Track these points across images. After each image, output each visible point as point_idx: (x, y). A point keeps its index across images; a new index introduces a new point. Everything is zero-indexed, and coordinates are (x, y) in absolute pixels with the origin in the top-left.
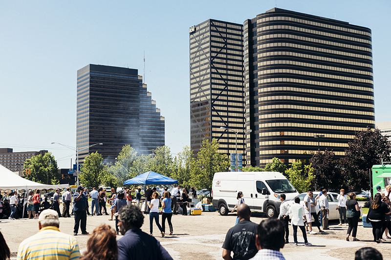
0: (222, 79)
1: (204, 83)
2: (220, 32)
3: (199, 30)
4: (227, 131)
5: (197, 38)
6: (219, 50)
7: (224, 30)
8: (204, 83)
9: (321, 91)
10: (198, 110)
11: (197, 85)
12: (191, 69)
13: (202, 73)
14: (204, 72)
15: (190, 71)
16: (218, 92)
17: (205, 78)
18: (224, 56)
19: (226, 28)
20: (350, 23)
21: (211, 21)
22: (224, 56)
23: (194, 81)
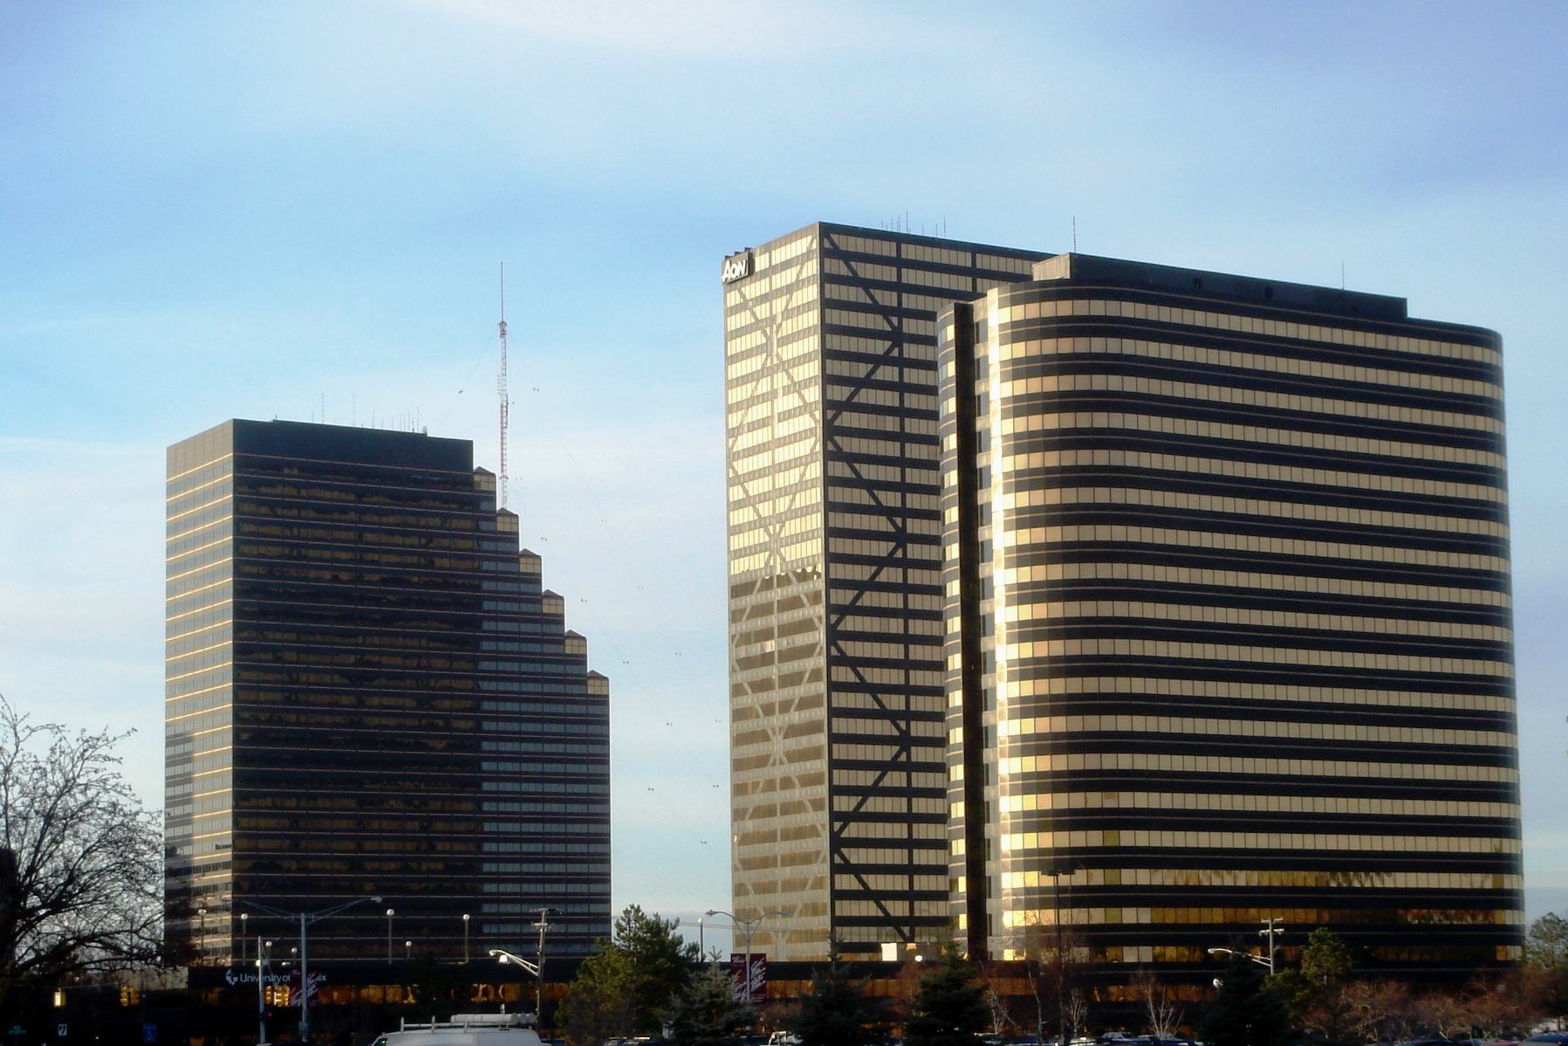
0: (878, 510)
1: (794, 527)
2: (867, 285)
3: (772, 270)
4: (895, 353)
5: (757, 310)
6: (862, 370)
7: (889, 274)
8: (794, 527)
9: (1319, 800)
10: (768, 862)
11: (759, 536)
12: (732, 456)
13: (783, 480)
14: (793, 476)
15: (730, 465)
16: (866, 778)
17: (797, 505)
18: (889, 399)
19: (899, 263)
20: (1413, 312)
21: (826, 230)
22: (889, 399)
23: (744, 515)
